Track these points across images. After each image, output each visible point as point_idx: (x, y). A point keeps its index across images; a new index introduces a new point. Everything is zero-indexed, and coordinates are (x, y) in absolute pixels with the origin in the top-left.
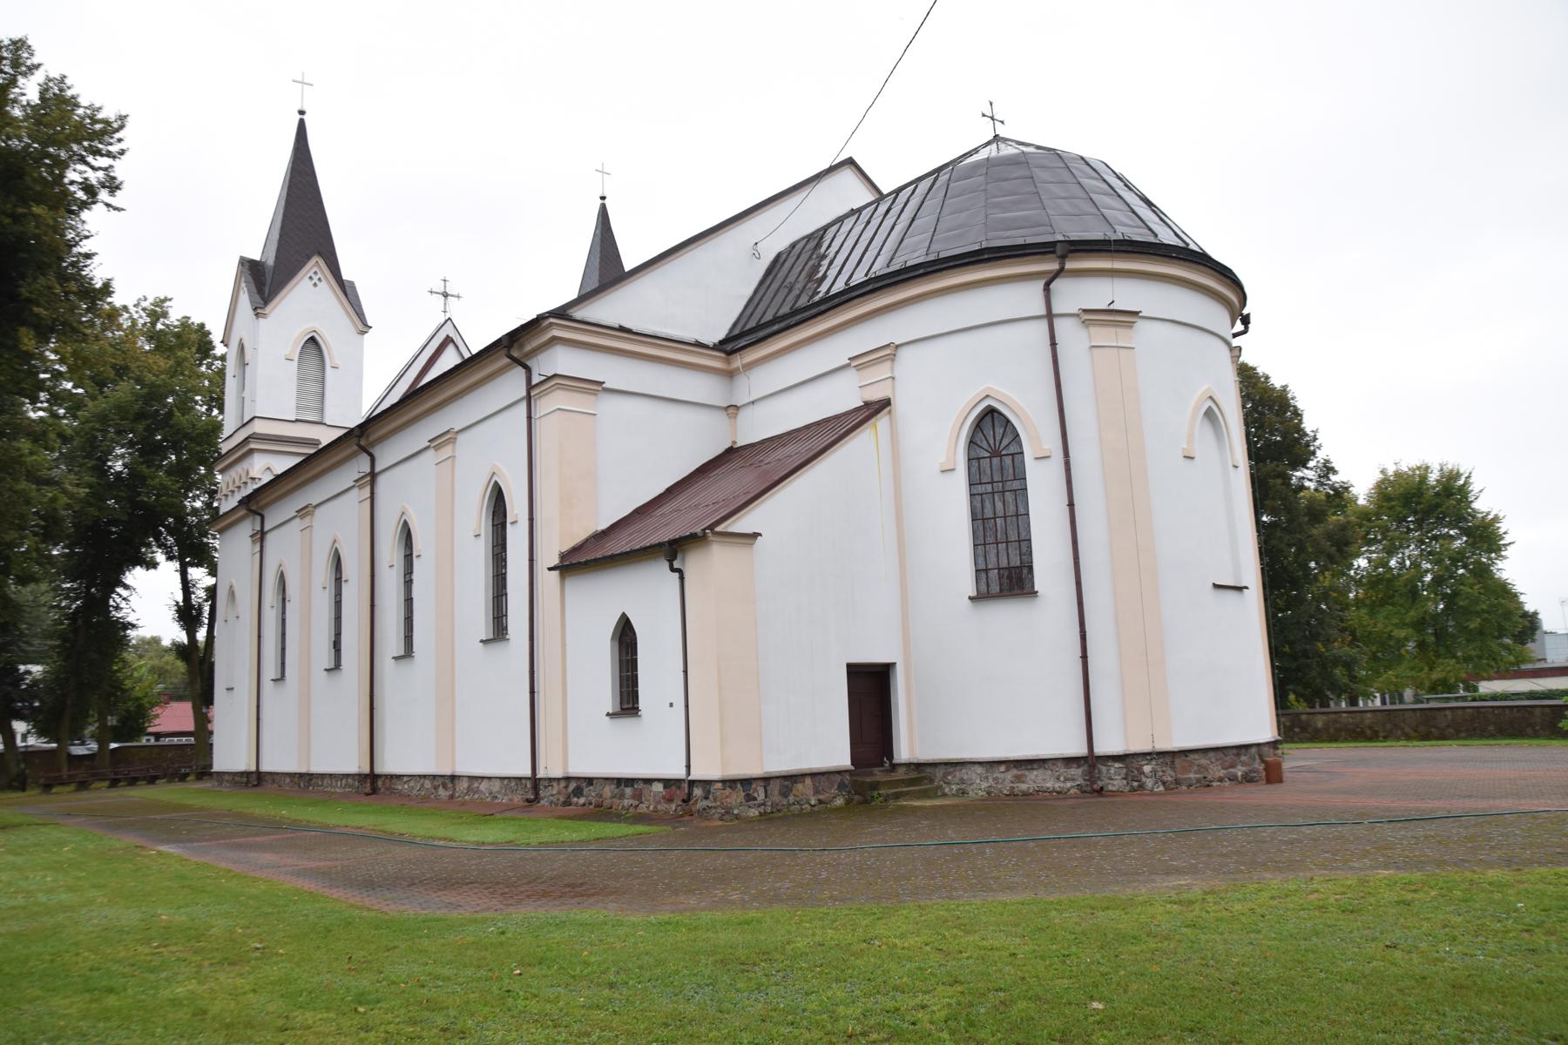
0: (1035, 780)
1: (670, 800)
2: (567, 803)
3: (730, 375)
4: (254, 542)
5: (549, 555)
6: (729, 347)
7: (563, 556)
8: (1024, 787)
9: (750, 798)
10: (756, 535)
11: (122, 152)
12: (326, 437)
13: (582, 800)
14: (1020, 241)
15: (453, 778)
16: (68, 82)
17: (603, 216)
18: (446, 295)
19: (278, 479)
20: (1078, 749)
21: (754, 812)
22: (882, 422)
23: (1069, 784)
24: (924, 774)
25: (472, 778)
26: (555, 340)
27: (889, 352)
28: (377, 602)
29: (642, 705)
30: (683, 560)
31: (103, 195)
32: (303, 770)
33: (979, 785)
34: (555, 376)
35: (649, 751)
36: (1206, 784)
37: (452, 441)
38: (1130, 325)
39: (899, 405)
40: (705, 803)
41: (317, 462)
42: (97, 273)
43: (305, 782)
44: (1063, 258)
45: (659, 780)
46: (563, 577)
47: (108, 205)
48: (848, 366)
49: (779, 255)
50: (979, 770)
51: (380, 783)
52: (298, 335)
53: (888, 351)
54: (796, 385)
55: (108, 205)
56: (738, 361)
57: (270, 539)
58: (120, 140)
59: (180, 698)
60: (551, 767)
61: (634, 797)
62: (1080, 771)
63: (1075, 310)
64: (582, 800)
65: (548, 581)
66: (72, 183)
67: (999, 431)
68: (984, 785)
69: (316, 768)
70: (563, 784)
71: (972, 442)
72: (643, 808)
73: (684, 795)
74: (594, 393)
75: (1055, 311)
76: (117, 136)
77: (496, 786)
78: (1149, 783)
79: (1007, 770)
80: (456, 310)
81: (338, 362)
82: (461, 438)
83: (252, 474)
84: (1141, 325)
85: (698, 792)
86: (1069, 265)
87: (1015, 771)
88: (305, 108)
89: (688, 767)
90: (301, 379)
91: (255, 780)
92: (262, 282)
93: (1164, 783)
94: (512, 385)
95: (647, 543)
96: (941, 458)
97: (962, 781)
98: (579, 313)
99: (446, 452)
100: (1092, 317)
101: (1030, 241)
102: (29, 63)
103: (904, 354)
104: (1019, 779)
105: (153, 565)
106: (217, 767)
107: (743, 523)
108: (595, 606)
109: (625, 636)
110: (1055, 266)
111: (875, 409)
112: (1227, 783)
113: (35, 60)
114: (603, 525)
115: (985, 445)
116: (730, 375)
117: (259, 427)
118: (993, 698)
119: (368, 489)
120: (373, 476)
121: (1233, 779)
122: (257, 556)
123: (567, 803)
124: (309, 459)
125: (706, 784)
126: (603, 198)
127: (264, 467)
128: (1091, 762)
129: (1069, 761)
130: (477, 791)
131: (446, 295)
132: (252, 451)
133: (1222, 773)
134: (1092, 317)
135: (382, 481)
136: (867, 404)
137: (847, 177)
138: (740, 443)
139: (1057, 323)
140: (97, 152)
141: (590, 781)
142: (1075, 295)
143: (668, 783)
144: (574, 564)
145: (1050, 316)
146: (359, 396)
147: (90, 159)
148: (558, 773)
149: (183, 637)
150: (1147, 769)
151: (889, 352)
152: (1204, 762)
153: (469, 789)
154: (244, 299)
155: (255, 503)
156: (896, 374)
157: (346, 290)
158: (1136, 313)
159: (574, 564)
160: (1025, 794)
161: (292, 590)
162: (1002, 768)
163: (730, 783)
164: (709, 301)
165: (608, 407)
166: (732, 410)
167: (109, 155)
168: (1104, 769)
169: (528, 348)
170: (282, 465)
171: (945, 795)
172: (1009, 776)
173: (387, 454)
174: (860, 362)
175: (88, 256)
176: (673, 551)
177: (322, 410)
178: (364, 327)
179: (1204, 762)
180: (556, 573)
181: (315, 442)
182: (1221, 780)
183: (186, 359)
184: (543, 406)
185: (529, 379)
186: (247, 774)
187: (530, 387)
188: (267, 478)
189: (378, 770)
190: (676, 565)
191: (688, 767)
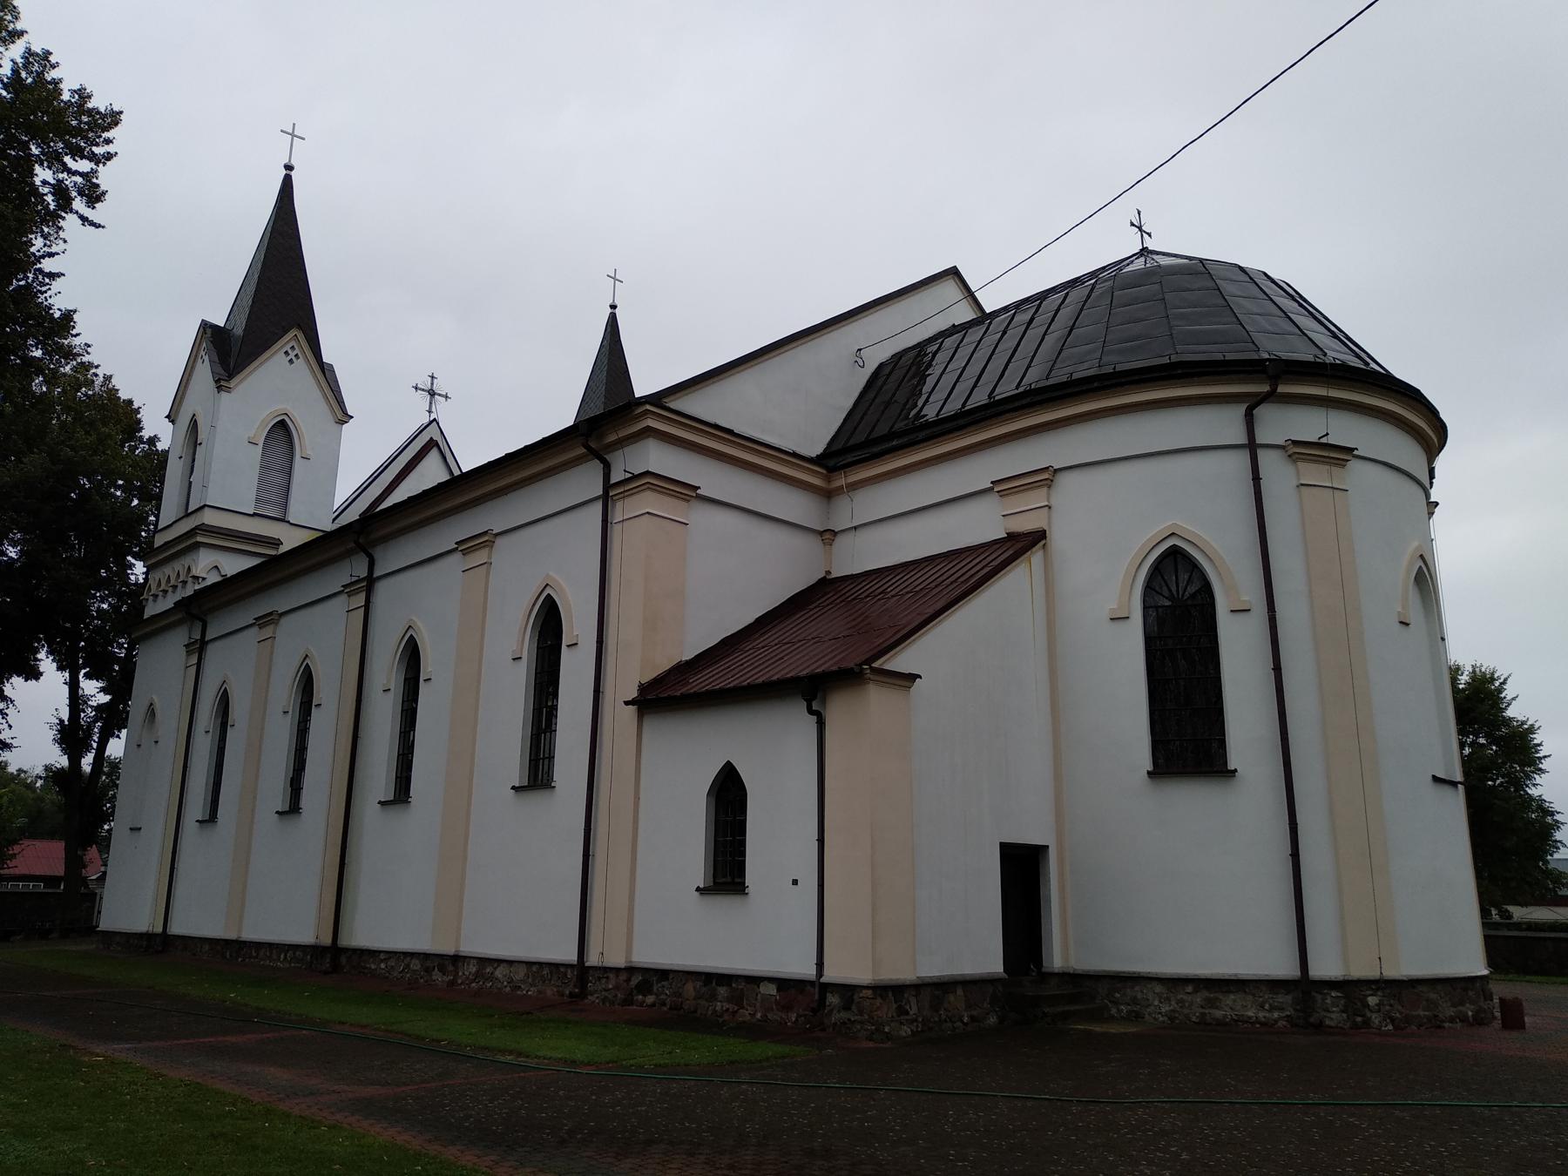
0: (1231, 1006)
1: (787, 1008)
2: (628, 1001)
3: (828, 495)
4: (189, 653)
5: (625, 682)
6: (831, 463)
7: (643, 688)
8: (1218, 1014)
9: (902, 1011)
10: (913, 677)
11: (109, 157)
12: (291, 540)
13: (650, 999)
14: (1219, 357)
15: (457, 959)
16: (53, 59)
17: (612, 326)
18: (432, 393)
19: (228, 583)
20: (1281, 966)
21: (906, 1031)
22: (1036, 557)
23: (1276, 1015)
24: (1082, 984)
25: (484, 961)
26: (649, 432)
27: (1046, 478)
28: (361, 734)
29: (749, 879)
30: (824, 703)
31: (79, 204)
32: (232, 936)
33: (1159, 1008)
34: (647, 473)
35: (764, 937)
36: (1436, 1024)
37: (489, 544)
38: (1342, 463)
39: (1057, 538)
40: (844, 1015)
41: (277, 570)
42: (59, 298)
43: (233, 955)
44: (1275, 380)
45: (771, 980)
46: (641, 715)
47: (84, 219)
48: (990, 489)
49: (881, 366)
50: (1158, 988)
51: (343, 960)
52: (258, 426)
53: (1046, 476)
54: (915, 514)
55: (84, 219)
56: (841, 481)
57: (212, 652)
58: (108, 142)
59: (51, 835)
60: (607, 952)
61: (729, 1000)
62: (1289, 998)
63: (1281, 442)
64: (650, 999)
65: (619, 718)
66: (45, 182)
67: (1184, 577)
68: (1165, 1008)
69: (249, 935)
70: (623, 977)
71: (1149, 588)
72: (745, 1015)
73: (808, 1006)
74: (686, 499)
75: (1260, 439)
76: (105, 135)
77: (416, 965)
78: (1376, 1019)
79: (1196, 991)
80: (443, 411)
81: (309, 452)
82: (500, 541)
83: (194, 572)
84: (1354, 465)
85: (833, 999)
86: (1281, 389)
87: (1206, 994)
88: (293, 162)
89: (820, 965)
90: (264, 467)
91: (159, 945)
92: (225, 352)
93: (1393, 1020)
94: (585, 482)
95: (776, 674)
96: (1111, 604)
97: (1135, 1001)
98: (691, 405)
99: (480, 557)
100: (1299, 451)
101: (1229, 357)
102: (11, 27)
103: (1065, 480)
104: (1211, 1003)
105: (33, 674)
106: (104, 925)
107: (900, 661)
108: (685, 757)
109: (728, 795)
110: (1266, 388)
111: (1022, 544)
112: (1459, 1025)
113: (19, 26)
114: (688, 655)
115: (1166, 593)
116: (828, 495)
117: (209, 518)
118: (1188, 897)
119: (363, 596)
120: (370, 583)
121: (1464, 1019)
122: (193, 670)
123: (628, 1001)
124: (272, 563)
125: (848, 991)
126: (613, 307)
127: (211, 566)
128: (1304, 988)
129: (1276, 985)
130: (491, 977)
131: (432, 393)
132: (198, 545)
133: (1451, 1012)
134: (1299, 451)
135: (382, 589)
136: (1012, 537)
137: (950, 289)
138: (834, 575)
139: (1261, 454)
140: (78, 153)
141: (663, 974)
142: (1279, 424)
143: (783, 984)
144: (666, 696)
145: (1252, 446)
146: (332, 494)
147: (67, 159)
148: (617, 960)
149: (63, 761)
150: (1372, 1001)
151: (1046, 478)
152: (1433, 996)
153: (478, 975)
154: (204, 371)
155: (202, 607)
156: (1053, 503)
157: (326, 372)
158: (1350, 450)
159: (666, 696)
160: (1221, 1023)
161: (238, 712)
162: (1190, 989)
163: (883, 990)
164: (806, 412)
165: (701, 517)
166: (828, 536)
167: (93, 158)
168: (1319, 997)
169: (612, 438)
170: (233, 565)
171: (1112, 1019)
172: (1198, 999)
173: (391, 557)
174: (1004, 487)
175: (53, 276)
176: (814, 690)
177: (285, 506)
178: (344, 417)
179: (1433, 996)
180: (632, 708)
181: (277, 543)
182: (1452, 1020)
183: (109, 435)
184: (619, 512)
185: (607, 476)
186: (148, 936)
187: (607, 486)
188: (213, 579)
189: (346, 941)
190: (815, 707)
191: (820, 965)
